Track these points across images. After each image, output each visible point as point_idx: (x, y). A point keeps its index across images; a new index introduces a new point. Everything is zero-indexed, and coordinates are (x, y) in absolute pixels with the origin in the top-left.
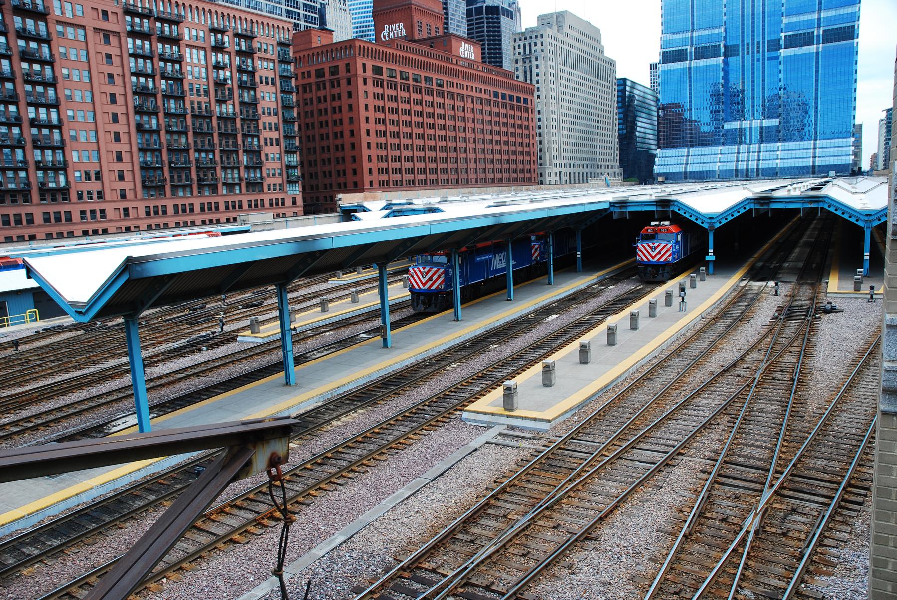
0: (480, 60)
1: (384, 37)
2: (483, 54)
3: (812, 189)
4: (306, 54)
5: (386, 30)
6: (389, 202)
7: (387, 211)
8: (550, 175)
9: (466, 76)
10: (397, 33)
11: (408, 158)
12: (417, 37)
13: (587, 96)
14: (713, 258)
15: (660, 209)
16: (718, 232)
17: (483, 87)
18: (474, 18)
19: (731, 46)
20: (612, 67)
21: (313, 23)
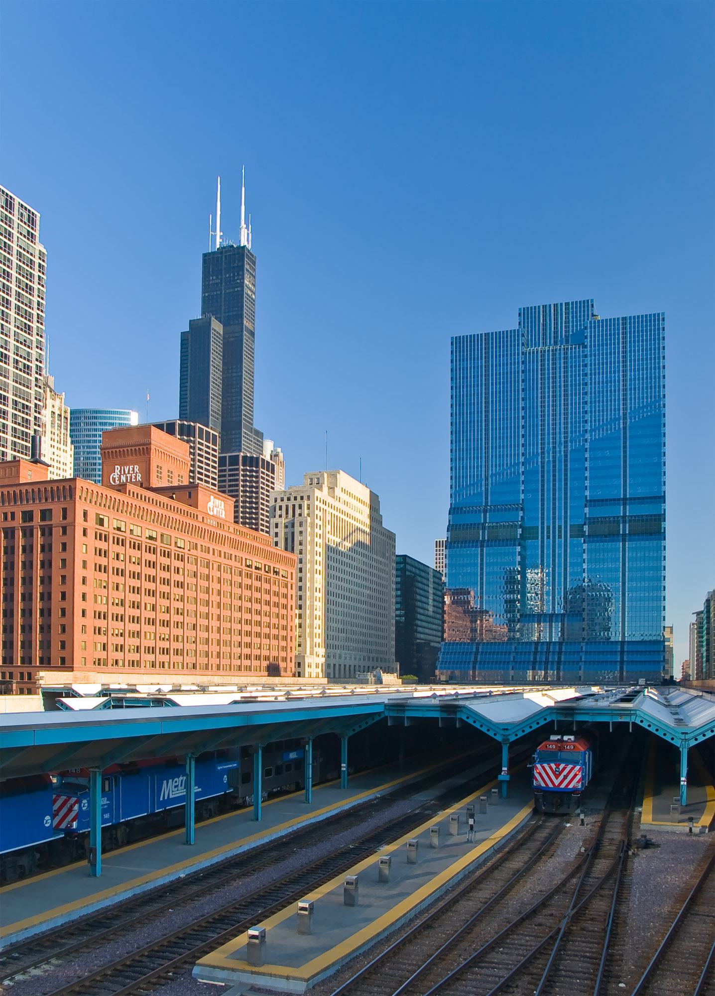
0: (232, 520)
1: (114, 479)
2: (236, 512)
3: (623, 700)
4: (11, 490)
5: (117, 471)
6: (106, 687)
7: (103, 699)
8: (310, 666)
9: (213, 537)
10: (131, 477)
11: (133, 633)
12: (155, 483)
13: (359, 573)
14: (507, 778)
15: (445, 715)
16: (513, 745)
17: (234, 552)
18: (227, 468)
19: (530, 528)
20: (391, 542)
21: (22, 453)
